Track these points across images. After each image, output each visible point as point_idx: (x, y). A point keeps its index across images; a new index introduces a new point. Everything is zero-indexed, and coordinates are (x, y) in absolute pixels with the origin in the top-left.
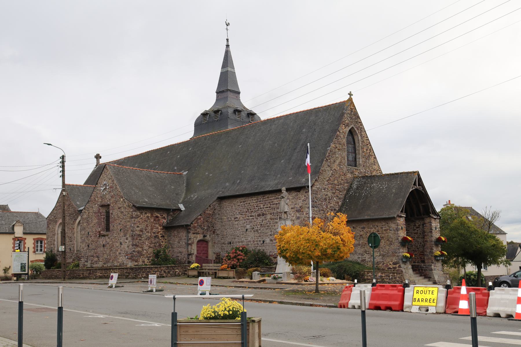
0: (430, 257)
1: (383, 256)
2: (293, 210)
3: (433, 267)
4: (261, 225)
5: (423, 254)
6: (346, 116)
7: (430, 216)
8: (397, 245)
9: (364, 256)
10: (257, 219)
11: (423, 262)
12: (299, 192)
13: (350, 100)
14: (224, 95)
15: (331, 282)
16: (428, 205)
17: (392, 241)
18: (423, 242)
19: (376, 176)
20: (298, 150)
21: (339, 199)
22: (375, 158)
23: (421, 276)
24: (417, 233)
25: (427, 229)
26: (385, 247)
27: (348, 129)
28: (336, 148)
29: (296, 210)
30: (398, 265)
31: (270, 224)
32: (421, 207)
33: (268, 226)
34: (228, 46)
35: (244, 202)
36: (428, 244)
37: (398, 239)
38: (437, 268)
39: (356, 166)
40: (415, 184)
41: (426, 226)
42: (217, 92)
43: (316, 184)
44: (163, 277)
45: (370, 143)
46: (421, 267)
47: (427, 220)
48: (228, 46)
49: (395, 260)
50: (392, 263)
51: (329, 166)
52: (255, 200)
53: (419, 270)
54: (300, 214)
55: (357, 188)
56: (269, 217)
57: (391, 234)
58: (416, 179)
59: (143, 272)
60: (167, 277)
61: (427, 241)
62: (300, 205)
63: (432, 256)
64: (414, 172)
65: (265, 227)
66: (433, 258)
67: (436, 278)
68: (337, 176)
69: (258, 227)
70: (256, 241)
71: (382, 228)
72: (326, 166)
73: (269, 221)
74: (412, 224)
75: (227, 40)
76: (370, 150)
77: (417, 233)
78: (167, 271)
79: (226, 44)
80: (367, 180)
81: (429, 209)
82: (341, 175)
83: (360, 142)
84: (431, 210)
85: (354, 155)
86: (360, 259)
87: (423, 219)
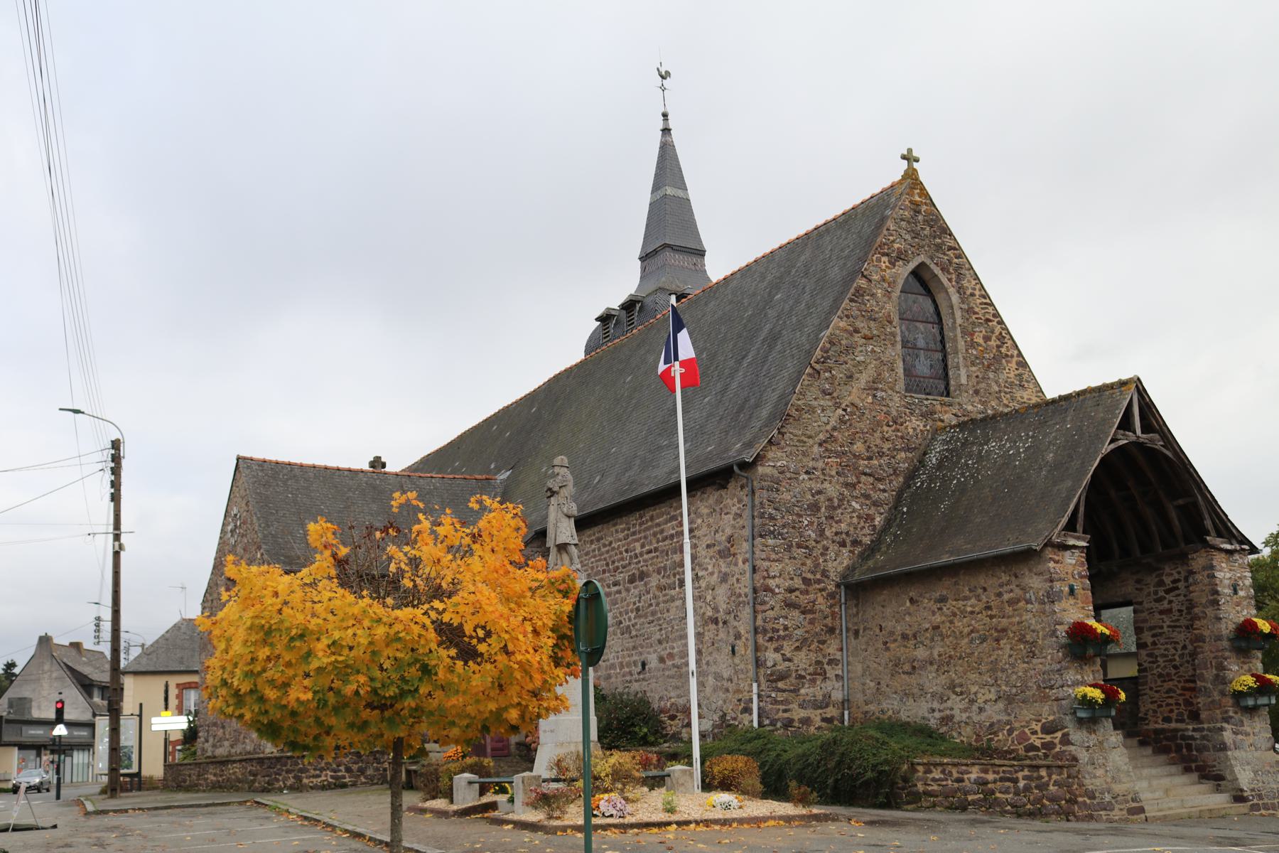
0: (1216, 696)
1: (1010, 699)
2: (711, 551)
4: (638, 609)
5: (1191, 686)
6: (891, 224)
8: (1051, 654)
9: (949, 704)
10: (628, 590)
11: (1195, 716)
12: (724, 487)
13: (911, 179)
14: (659, 260)
15: (719, 814)
16: (1195, 504)
17: (1034, 643)
18: (1192, 642)
19: (1002, 415)
20: (749, 358)
21: (875, 504)
22: (1023, 364)
23: (1187, 770)
24: (1168, 611)
26: (1013, 665)
27: (903, 270)
28: (857, 331)
29: (719, 552)
30: (1059, 734)
31: (658, 604)
32: (1173, 515)
33: (653, 613)
34: (666, 131)
35: (598, 540)
36: (1206, 647)
37: (1053, 633)
38: (1251, 739)
39: (948, 395)
40: (1126, 424)
41: (1195, 583)
42: (643, 259)
43: (770, 455)
44: (344, 786)
46: (1184, 738)
47: (1198, 561)
48: (666, 131)
49: (1048, 713)
50: (1038, 728)
51: (825, 392)
52: (623, 531)
53: (1179, 749)
54: (729, 565)
55: (940, 466)
56: (654, 581)
57: (1030, 617)
58: (1135, 407)
59: (288, 772)
60: (354, 785)
61: (1200, 639)
62: (728, 531)
63: (1223, 693)
64: (1123, 384)
65: (645, 616)
67: (1245, 778)
68: (864, 425)
69: (630, 619)
70: (628, 665)
71: (999, 595)
72: (814, 392)
73: (655, 597)
74: (1151, 580)
75: (665, 115)
76: (1001, 338)
77: (1169, 611)
78: (355, 767)
79: (661, 125)
80: (972, 432)
81: (1202, 519)
82: (879, 424)
83: (958, 314)
84: (1208, 523)
85: (939, 356)
86: (937, 715)
87: (1183, 558)
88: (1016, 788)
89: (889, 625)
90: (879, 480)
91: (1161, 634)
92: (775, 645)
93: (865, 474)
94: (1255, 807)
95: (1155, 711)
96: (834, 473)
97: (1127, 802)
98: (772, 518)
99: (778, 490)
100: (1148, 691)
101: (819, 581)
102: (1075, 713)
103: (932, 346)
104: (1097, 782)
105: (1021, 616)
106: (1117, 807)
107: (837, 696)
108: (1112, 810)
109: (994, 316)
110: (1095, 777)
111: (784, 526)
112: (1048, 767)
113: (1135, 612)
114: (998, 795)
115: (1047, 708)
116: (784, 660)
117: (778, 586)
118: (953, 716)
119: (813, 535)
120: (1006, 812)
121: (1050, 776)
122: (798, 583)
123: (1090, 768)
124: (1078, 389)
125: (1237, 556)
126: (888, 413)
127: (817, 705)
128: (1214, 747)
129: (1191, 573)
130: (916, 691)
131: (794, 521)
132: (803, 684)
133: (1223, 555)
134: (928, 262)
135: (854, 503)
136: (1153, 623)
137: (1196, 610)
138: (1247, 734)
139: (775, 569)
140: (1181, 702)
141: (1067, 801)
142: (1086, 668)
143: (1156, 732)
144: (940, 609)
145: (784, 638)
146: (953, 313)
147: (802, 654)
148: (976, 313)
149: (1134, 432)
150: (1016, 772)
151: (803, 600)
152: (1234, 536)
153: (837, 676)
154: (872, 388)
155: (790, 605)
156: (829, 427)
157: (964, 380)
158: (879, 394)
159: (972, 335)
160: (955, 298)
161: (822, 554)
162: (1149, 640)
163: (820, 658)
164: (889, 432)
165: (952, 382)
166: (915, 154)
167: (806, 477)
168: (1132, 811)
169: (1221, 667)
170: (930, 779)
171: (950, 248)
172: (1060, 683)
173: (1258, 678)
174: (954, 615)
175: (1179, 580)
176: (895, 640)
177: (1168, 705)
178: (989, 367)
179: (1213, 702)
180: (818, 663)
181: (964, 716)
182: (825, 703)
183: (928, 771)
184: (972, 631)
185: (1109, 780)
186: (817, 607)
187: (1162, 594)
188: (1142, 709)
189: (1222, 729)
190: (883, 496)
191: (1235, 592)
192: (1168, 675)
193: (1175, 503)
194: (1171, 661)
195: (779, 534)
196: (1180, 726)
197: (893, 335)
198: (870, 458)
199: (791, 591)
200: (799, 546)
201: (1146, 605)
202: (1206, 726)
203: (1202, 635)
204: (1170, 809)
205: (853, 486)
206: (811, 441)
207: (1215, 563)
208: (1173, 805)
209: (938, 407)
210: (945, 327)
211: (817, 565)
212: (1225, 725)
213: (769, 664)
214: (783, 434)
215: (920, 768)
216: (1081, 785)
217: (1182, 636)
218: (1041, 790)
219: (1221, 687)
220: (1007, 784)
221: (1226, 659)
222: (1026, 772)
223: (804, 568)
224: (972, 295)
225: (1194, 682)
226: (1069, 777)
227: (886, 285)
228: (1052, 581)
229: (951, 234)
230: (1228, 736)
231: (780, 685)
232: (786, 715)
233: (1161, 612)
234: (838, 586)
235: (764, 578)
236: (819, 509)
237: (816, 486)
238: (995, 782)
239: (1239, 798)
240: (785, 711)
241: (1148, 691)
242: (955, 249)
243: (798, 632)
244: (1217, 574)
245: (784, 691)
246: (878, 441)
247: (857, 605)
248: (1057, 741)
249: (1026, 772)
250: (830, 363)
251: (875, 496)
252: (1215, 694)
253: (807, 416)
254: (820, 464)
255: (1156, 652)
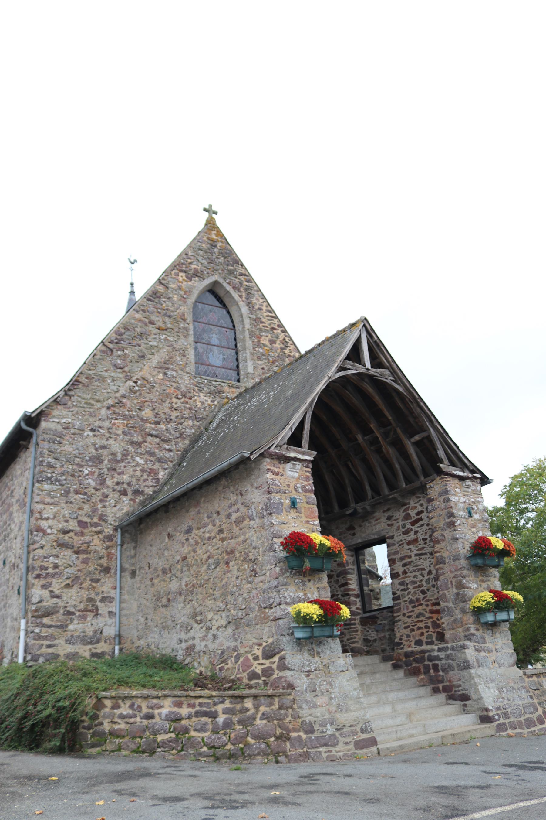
0: (458, 614)
3: (470, 653)
7: (440, 472)
11: (441, 637)
13: (211, 225)
16: (429, 438)
25: (438, 521)
26: (239, 587)
28: (152, 323)
30: (276, 659)
32: (412, 450)
36: (447, 568)
37: (271, 548)
38: (494, 656)
40: (355, 354)
41: (434, 510)
45: (281, 326)
46: (430, 659)
47: (435, 487)
49: (267, 634)
50: (259, 653)
51: (116, 367)
53: (427, 670)
58: (365, 347)
61: (441, 561)
63: (463, 611)
66: (470, 618)
67: (489, 696)
68: (154, 396)
71: (229, 516)
74: (399, 514)
75: (132, 284)
76: (284, 341)
77: (416, 541)
81: (436, 450)
82: (168, 396)
83: (247, 321)
84: (441, 453)
88: (214, 724)
89: (154, 561)
90: (166, 441)
91: (410, 563)
92: (42, 582)
93: (152, 435)
94: (501, 727)
95: (408, 636)
96: (120, 432)
97: (355, 733)
98: (50, 466)
99: (60, 443)
100: (401, 617)
101: (96, 525)
102: (293, 634)
103: (224, 343)
104: (318, 712)
105: (244, 534)
106: (342, 740)
107: (110, 631)
108: (335, 745)
109: (278, 326)
110: (315, 706)
111: (63, 474)
112: (255, 697)
113: (388, 546)
114: (193, 733)
115: (267, 629)
116: (52, 597)
117: (51, 527)
118: (194, 646)
119: (93, 484)
120: (200, 754)
121: (257, 708)
122: (73, 525)
123: (309, 696)
124: (318, 343)
125: (468, 482)
126: (177, 388)
127: (86, 641)
128: (458, 665)
129: (430, 500)
130: (170, 623)
131: (73, 470)
132: (72, 620)
133: (457, 481)
134: (221, 281)
135: (138, 459)
136: (402, 554)
137: (436, 534)
138: (490, 651)
139: (49, 511)
140: (430, 624)
141: (277, 738)
142: (310, 584)
143: (407, 655)
144: (187, 540)
145: (53, 576)
146: (243, 321)
147: (73, 592)
148: (262, 322)
149: (364, 365)
150: (215, 704)
151: (77, 541)
152: (467, 467)
153: (110, 613)
154: (164, 367)
155: (63, 545)
156: (118, 395)
157: (250, 370)
158: (169, 373)
159: (259, 337)
160: (244, 310)
161: (101, 501)
162: (400, 570)
163: (93, 596)
164: (178, 403)
165: (242, 372)
166: (214, 209)
167: (91, 434)
168: (360, 745)
169: (460, 586)
170: (117, 716)
171: (241, 275)
172: (277, 600)
173: (496, 593)
174: (197, 543)
175: (422, 512)
176: (158, 576)
177: (419, 628)
178: (273, 362)
179: (456, 620)
180: (90, 600)
181: (203, 644)
182: (97, 637)
183: (116, 707)
184: (209, 557)
185: (333, 709)
186: (92, 548)
187: (408, 526)
188: (398, 635)
189: (464, 647)
190: (168, 454)
191: (470, 515)
192: (418, 600)
193: (413, 440)
194: (419, 586)
195: (57, 480)
196: (429, 647)
197: (187, 330)
198: (158, 423)
199: (65, 532)
200: (77, 492)
201: (397, 539)
202: (449, 645)
203: (442, 557)
204: (411, 736)
205: (139, 444)
206: (99, 405)
207: (449, 488)
208: (414, 732)
209: (226, 388)
210: (237, 332)
211: (95, 510)
212: (467, 643)
213: (35, 600)
214: (70, 397)
215: (108, 703)
216: (296, 717)
217: (427, 563)
218: (245, 726)
219: (461, 605)
220: (205, 719)
221: (464, 577)
222: (228, 704)
223: (80, 512)
224: (260, 309)
225: (438, 604)
226: (280, 708)
227: (182, 293)
228: (269, 492)
229: (242, 265)
230: (470, 653)
231: (46, 620)
232: (50, 650)
233: (409, 543)
234: (115, 530)
235: (37, 519)
236: (101, 462)
237: (100, 442)
238: (189, 717)
239: (485, 719)
240: (49, 646)
241: (401, 617)
242: (245, 275)
243: (70, 571)
244: (451, 498)
245: (50, 627)
246: (167, 410)
247: (135, 548)
248: (274, 666)
249: (228, 704)
250: (124, 344)
251: (160, 454)
252: (457, 612)
253: (97, 383)
254: (107, 424)
255: (407, 580)
